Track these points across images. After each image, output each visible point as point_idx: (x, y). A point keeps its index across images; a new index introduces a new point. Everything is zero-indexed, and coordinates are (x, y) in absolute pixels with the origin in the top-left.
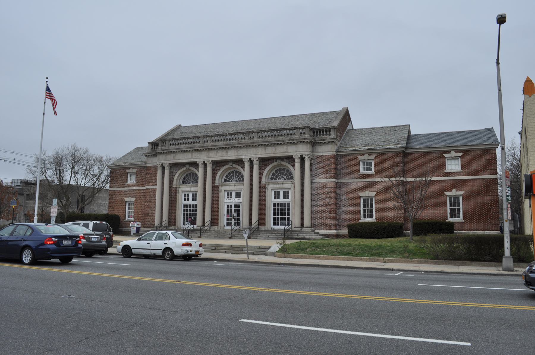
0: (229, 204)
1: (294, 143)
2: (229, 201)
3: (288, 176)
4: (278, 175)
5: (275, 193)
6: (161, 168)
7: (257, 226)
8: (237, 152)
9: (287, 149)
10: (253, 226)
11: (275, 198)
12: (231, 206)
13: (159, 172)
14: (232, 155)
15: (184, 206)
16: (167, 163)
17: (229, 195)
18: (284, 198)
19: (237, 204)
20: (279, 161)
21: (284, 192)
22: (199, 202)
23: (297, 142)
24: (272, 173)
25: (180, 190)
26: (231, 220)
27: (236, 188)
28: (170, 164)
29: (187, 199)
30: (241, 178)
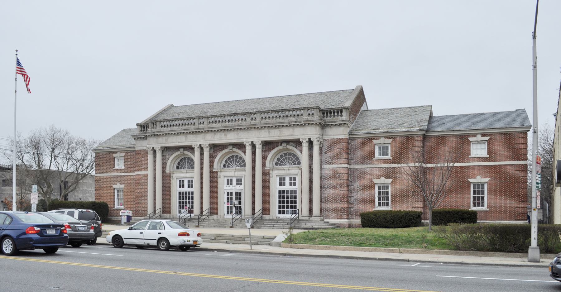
0: (230, 191)
1: (301, 125)
2: (229, 188)
3: (294, 161)
4: (284, 159)
5: (280, 179)
7: (261, 215)
8: (238, 135)
11: (280, 185)
13: (150, 157)
17: (229, 182)
21: (291, 179)
22: (195, 189)
24: (277, 157)
25: (175, 176)
26: (231, 208)
27: (237, 174)
28: (209, 144)
29: (182, 186)
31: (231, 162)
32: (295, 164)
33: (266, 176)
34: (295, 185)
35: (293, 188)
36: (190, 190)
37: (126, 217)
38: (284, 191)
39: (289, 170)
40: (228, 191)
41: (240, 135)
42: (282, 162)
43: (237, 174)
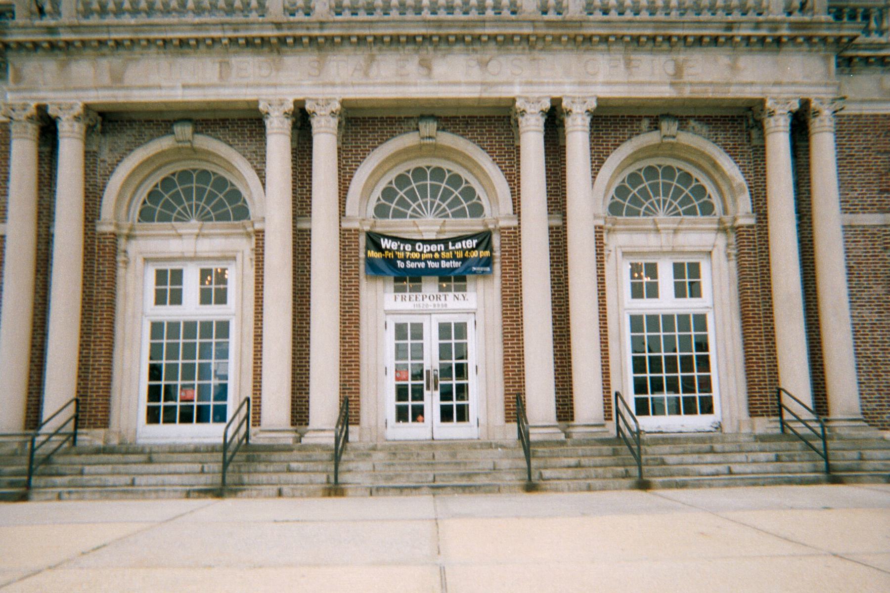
0: (409, 320)
1: (778, 41)
2: (408, 305)
3: (221, 204)
4: (643, 192)
5: (161, 276)
6: (32, 130)
7: (70, 428)
8: (483, 64)
9: (733, 67)
10: (47, 428)
11: (160, 299)
12: (418, 332)
13: (23, 152)
14: (456, 78)
15: (157, 329)
16: (77, 100)
17: (169, 287)
18: (679, 292)
19: (453, 319)
20: (669, 127)
21: (678, 270)
22: (235, 310)
23: (793, 39)
24: (383, 185)
25: (135, 249)
26: (418, 394)
27: (206, 246)
28: (87, 107)
29: (643, 288)
30: (228, 205)
31: (412, 195)
32: (691, 212)
33: (101, 259)
34: (222, 298)
35: (689, 306)
36: (213, 313)
37: (758, 421)
38: (653, 320)
39: (676, 231)
40: (402, 319)
41: (493, 66)
42: (167, 205)
43: (206, 246)
